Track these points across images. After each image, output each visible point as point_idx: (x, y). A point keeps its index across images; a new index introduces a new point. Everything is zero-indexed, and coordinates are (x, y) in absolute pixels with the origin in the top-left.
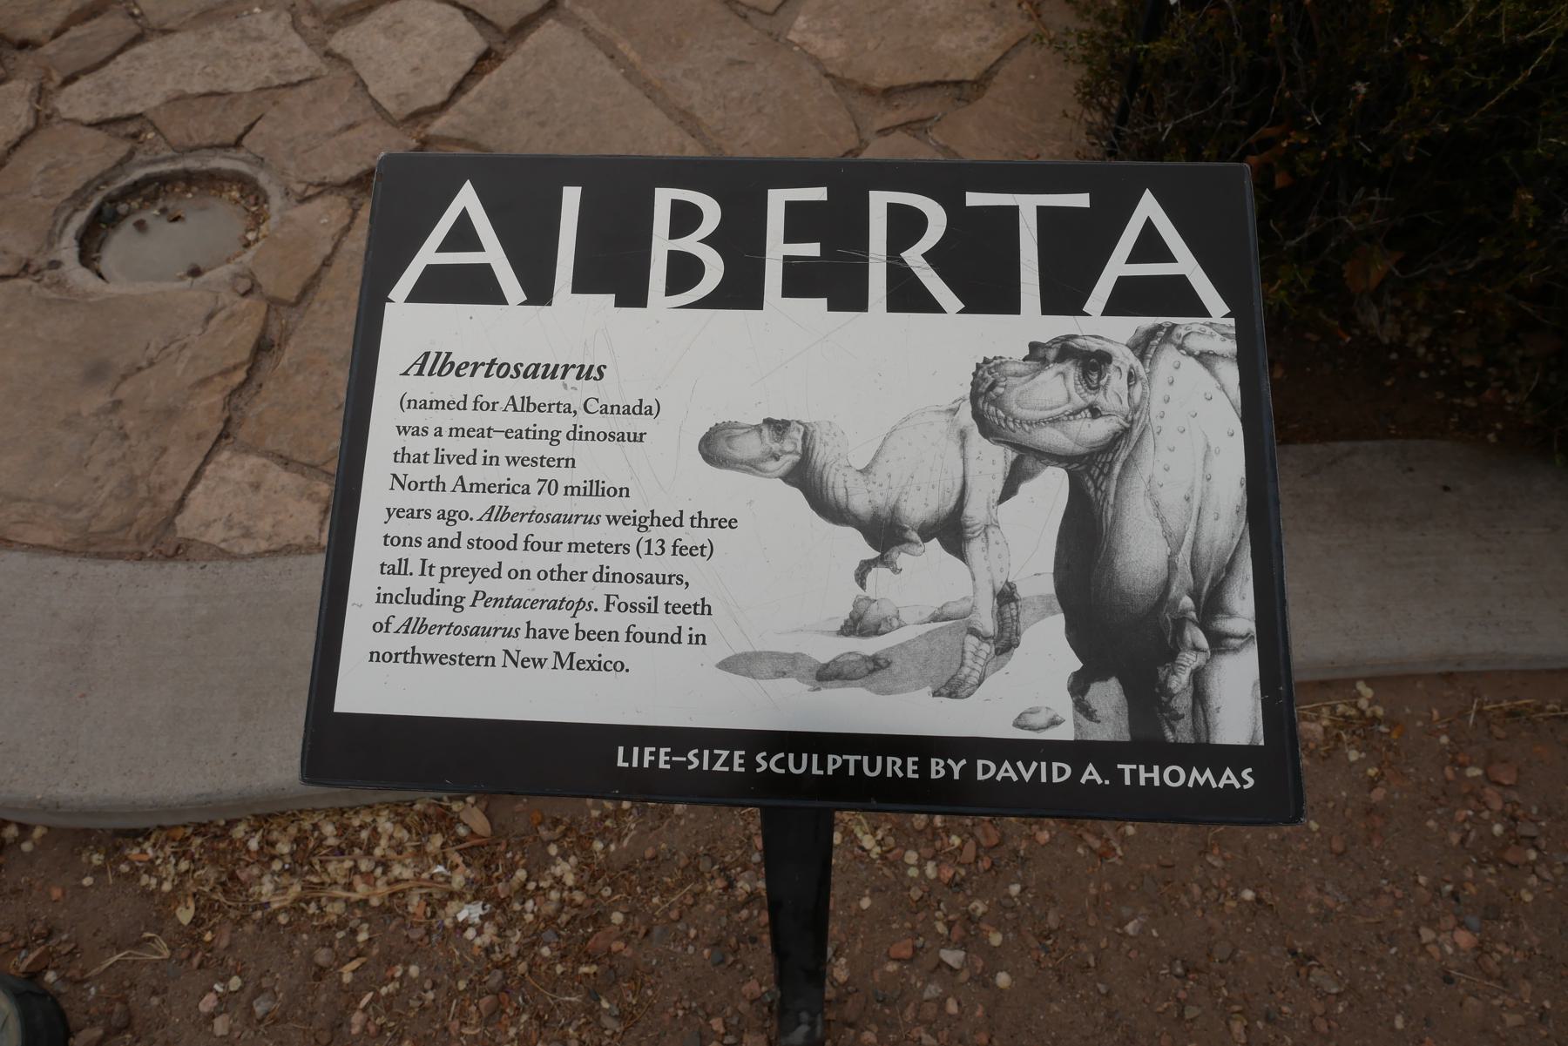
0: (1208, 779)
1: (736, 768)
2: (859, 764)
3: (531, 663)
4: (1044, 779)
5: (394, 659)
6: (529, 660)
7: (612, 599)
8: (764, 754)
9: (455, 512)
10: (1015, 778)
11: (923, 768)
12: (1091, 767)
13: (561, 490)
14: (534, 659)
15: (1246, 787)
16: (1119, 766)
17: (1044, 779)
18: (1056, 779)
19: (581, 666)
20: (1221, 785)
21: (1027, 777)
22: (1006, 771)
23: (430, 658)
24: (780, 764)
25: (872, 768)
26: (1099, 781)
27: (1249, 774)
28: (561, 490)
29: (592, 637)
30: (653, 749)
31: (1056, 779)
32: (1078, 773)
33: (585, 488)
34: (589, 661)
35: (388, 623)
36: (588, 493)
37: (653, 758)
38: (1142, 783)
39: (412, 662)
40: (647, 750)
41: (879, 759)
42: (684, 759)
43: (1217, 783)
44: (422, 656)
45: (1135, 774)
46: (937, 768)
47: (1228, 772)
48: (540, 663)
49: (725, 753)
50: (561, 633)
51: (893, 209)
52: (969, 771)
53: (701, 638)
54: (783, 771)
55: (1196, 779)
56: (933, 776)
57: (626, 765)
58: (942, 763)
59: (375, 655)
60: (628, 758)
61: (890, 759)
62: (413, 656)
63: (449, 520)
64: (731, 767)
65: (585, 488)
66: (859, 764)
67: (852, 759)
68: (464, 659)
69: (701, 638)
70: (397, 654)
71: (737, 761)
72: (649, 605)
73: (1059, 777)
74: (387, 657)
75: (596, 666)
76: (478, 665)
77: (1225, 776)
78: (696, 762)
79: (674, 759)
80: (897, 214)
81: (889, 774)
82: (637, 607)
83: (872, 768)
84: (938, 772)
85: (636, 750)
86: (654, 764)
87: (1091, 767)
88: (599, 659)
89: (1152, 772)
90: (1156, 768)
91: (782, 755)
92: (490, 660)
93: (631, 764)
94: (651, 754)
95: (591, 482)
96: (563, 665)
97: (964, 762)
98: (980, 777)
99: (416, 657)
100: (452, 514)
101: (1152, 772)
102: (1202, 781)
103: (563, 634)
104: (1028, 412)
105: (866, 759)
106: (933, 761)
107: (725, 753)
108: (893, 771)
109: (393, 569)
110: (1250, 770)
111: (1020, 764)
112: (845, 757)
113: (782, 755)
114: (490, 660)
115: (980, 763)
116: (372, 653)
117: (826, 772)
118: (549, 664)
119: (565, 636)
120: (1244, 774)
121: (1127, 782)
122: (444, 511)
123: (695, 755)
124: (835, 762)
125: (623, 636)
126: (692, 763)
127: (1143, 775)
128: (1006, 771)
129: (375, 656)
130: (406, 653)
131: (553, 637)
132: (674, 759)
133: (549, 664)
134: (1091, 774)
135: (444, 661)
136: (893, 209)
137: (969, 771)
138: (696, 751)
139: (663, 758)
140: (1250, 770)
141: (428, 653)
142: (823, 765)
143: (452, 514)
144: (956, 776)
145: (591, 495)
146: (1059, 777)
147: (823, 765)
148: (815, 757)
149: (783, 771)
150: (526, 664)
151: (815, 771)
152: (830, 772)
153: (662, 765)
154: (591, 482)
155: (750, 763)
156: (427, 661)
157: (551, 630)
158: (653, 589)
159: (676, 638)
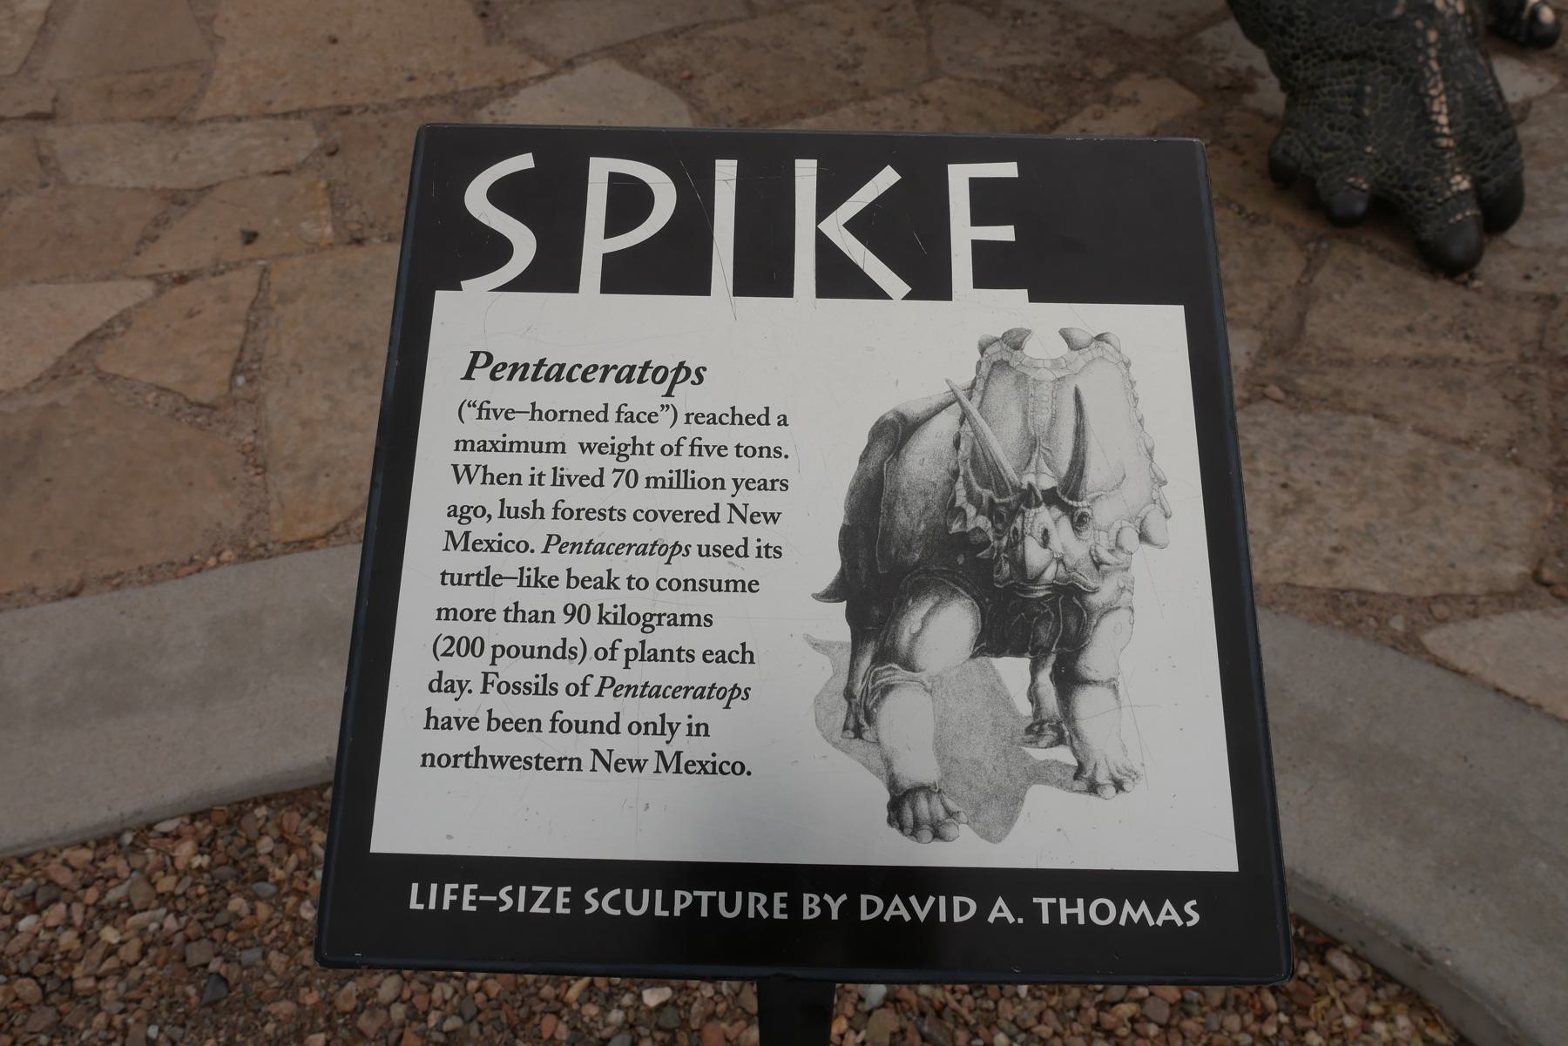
0: (1143, 914)
1: (560, 910)
2: (713, 902)
3: (627, 766)
4: (943, 918)
5: (452, 764)
6: (624, 762)
7: (491, 678)
8: (595, 890)
9: (469, 508)
10: (907, 918)
11: (794, 906)
12: (1000, 902)
13: (642, 482)
14: (630, 761)
15: (1190, 924)
16: (1035, 900)
17: (943, 918)
18: (957, 918)
19: (691, 769)
20: (1159, 922)
21: (922, 915)
22: (897, 908)
23: (499, 762)
24: (615, 903)
25: (730, 906)
26: (1011, 920)
27: (1193, 908)
28: (642, 482)
29: (508, 726)
30: (456, 886)
31: (957, 918)
32: (984, 909)
33: (671, 479)
34: (700, 762)
35: (585, 684)
36: (675, 485)
37: (455, 898)
38: (1064, 921)
39: (476, 766)
40: (448, 887)
41: (739, 895)
42: (494, 898)
43: (1155, 918)
44: (489, 759)
45: (1054, 909)
46: (810, 906)
47: (1168, 905)
48: (639, 765)
49: (546, 890)
50: (470, 722)
51: (614, 178)
52: (850, 909)
53: (702, 729)
54: (618, 912)
55: (1129, 914)
56: (806, 916)
57: (421, 907)
58: (817, 899)
59: (429, 759)
60: (423, 897)
61: (752, 895)
62: (476, 759)
63: (462, 517)
64: (553, 908)
65: (671, 479)
66: (713, 902)
67: (705, 895)
68: (542, 762)
69: (702, 729)
70: (456, 757)
71: (561, 900)
72: (537, 684)
73: (961, 915)
74: (444, 761)
75: (709, 768)
76: (560, 769)
77: (1164, 911)
78: (509, 902)
79: (482, 898)
80: (618, 183)
81: (751, 915)
82: (522, 687)
83: (730, 906)
84: (811, 911)
85: (434, 887)
86: (456, 905)
87: (1000, 902)
88: (712, 759)
89: (1076, 906)
90: (1080, 902)
91: (617, 892)
92: (575, 763)
93: (427, 905)
94: (453, 892)
95: (678, 471)
96: (667, 768)
97: (844, 897)
98: (864, 916)
99: (481, 760)
100: (465, 510)
101: (1076, 906)
102: (1136, 918)
103: (471, 723)
104: (991, 432)
105: (722, 895)
106: (806, 897)
107: (546, 890)
108: (756, 908)
109: (601, 582)
110: (1194, 902)
111: (913, 899)
112: (696, 893)
113: (617, 892)
114: (575, 763)
115: (864, 898)
116: (424, 756)
117: (672, 912)
118: (650, 767)
119: (474, 725)
120: (1188, 908)
121: (1045, 920)
122: (455, 507)
123: (508, 893)
124: (683, 899)
125: (546, 726)
126: (504, 903)
127: (1064, 911)
128: (897, 908)
129: (429, 760)
130: (468, 756)
131: (459, 727)
132: (482, 898)
133: (650, 767)
134: (1001, 910)
135: (516, 764)
136: (614, 178)
137: (850, 909)
138: (510, 888)
139: (467, 897)
140: (1194, 902)
141: (497, 754)
142: (668, 904)
143: (465, 510)
144: (835, 916)
145: (678, 487)
146: (961, 915)
147: (668, 904)
148: (659, 893)
149: (618, 912)
150: (621, 767)
151: (659, 912)
152: (677, 913)
153: (466, 907)
154: (678, 471)
155: (577, 902)
156: (495, 766)
157: (457, 719)
158: (542, 666)
159: (613, 727)
